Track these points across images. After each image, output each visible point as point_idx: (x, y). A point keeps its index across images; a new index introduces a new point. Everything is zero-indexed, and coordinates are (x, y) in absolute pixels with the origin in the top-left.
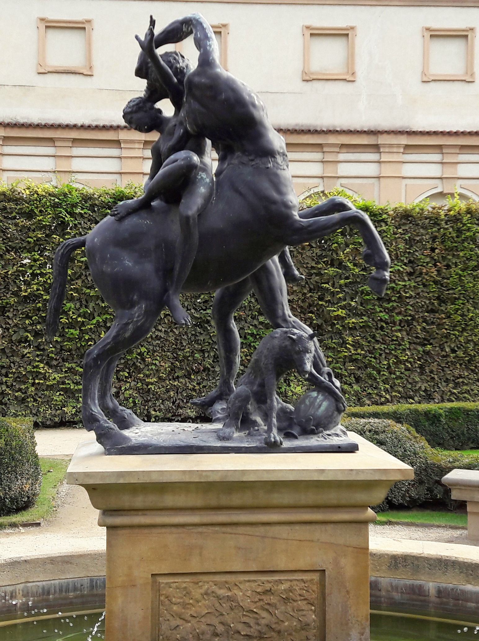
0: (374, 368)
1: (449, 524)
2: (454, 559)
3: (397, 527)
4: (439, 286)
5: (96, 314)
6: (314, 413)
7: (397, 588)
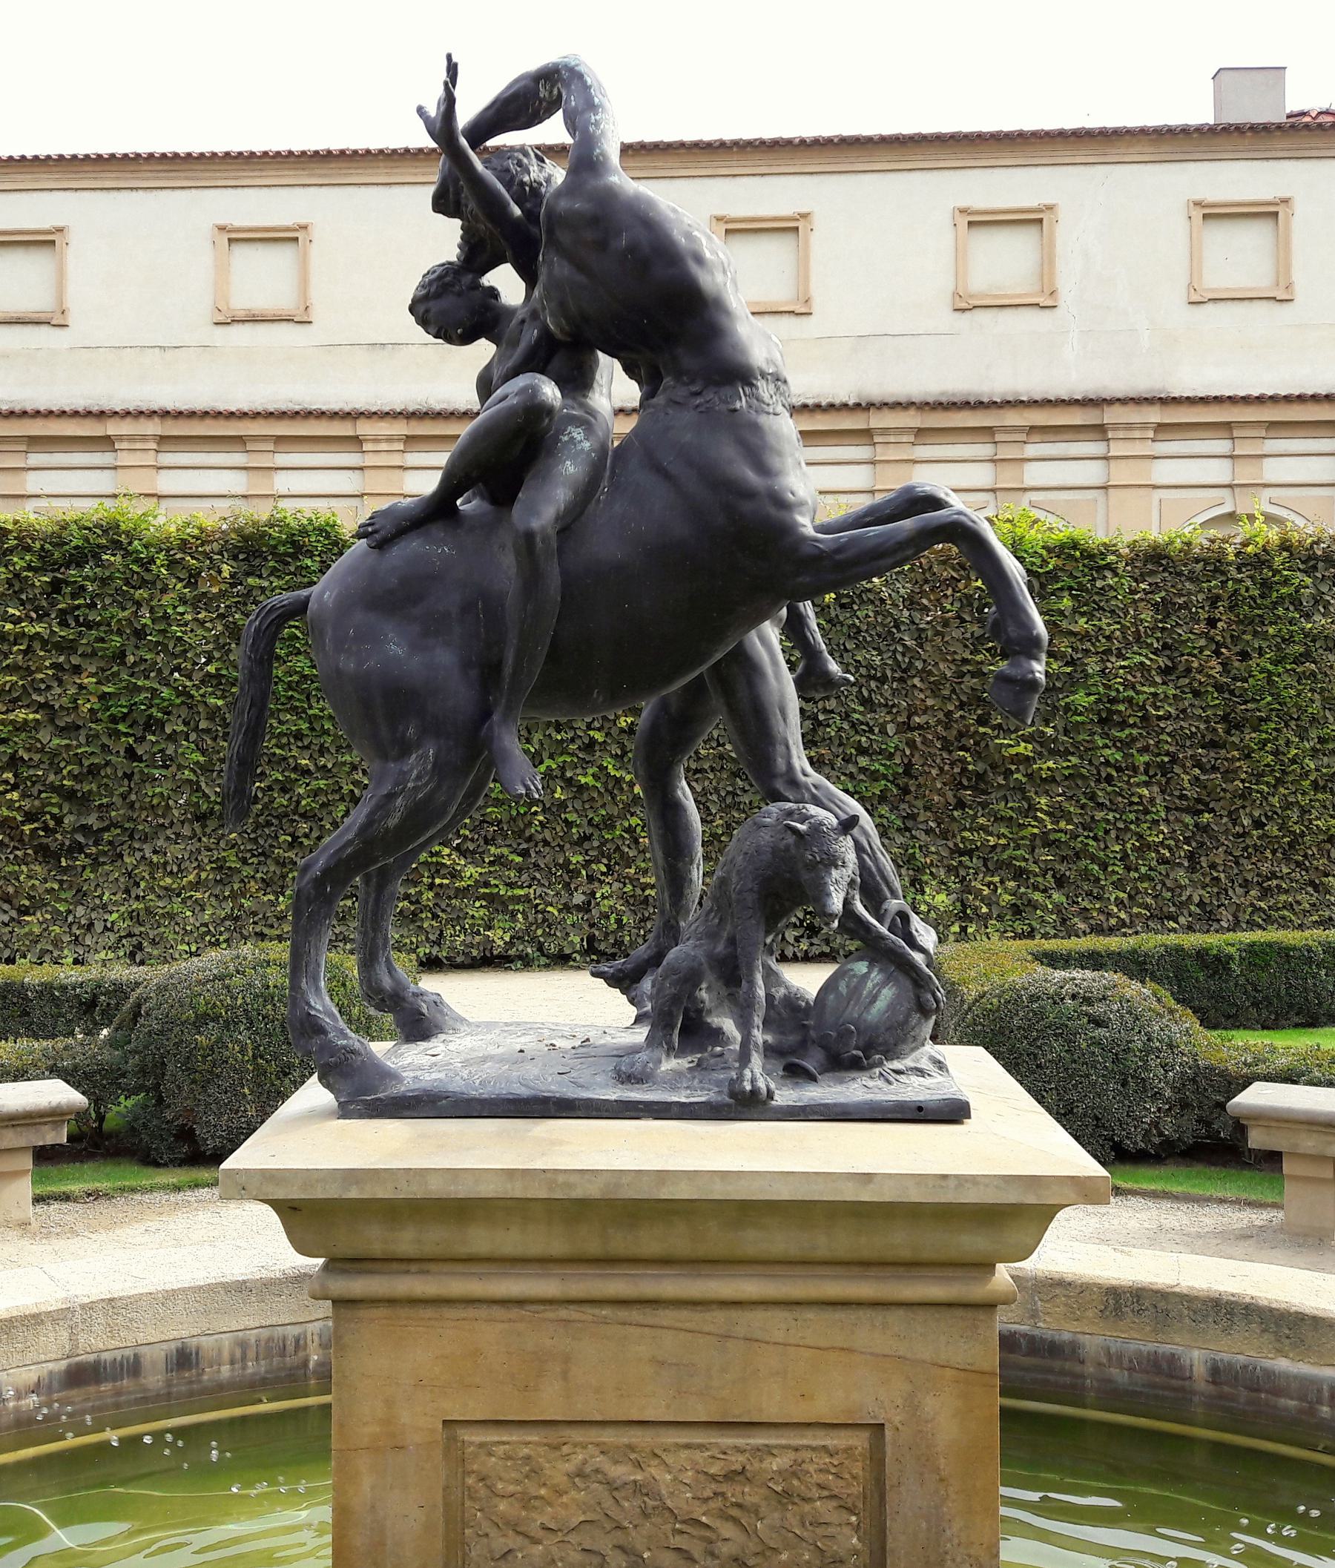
0: (1093, 859)
1: (1244, 1196)
2: (1248, 1300)
3: (1133, 1201)
4: (1226, 695)
5: (545, 755)
6: (860, 1015)
7: (1120, 1357)
